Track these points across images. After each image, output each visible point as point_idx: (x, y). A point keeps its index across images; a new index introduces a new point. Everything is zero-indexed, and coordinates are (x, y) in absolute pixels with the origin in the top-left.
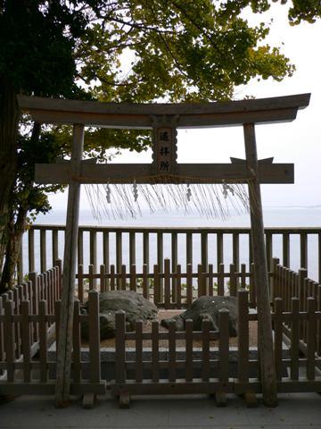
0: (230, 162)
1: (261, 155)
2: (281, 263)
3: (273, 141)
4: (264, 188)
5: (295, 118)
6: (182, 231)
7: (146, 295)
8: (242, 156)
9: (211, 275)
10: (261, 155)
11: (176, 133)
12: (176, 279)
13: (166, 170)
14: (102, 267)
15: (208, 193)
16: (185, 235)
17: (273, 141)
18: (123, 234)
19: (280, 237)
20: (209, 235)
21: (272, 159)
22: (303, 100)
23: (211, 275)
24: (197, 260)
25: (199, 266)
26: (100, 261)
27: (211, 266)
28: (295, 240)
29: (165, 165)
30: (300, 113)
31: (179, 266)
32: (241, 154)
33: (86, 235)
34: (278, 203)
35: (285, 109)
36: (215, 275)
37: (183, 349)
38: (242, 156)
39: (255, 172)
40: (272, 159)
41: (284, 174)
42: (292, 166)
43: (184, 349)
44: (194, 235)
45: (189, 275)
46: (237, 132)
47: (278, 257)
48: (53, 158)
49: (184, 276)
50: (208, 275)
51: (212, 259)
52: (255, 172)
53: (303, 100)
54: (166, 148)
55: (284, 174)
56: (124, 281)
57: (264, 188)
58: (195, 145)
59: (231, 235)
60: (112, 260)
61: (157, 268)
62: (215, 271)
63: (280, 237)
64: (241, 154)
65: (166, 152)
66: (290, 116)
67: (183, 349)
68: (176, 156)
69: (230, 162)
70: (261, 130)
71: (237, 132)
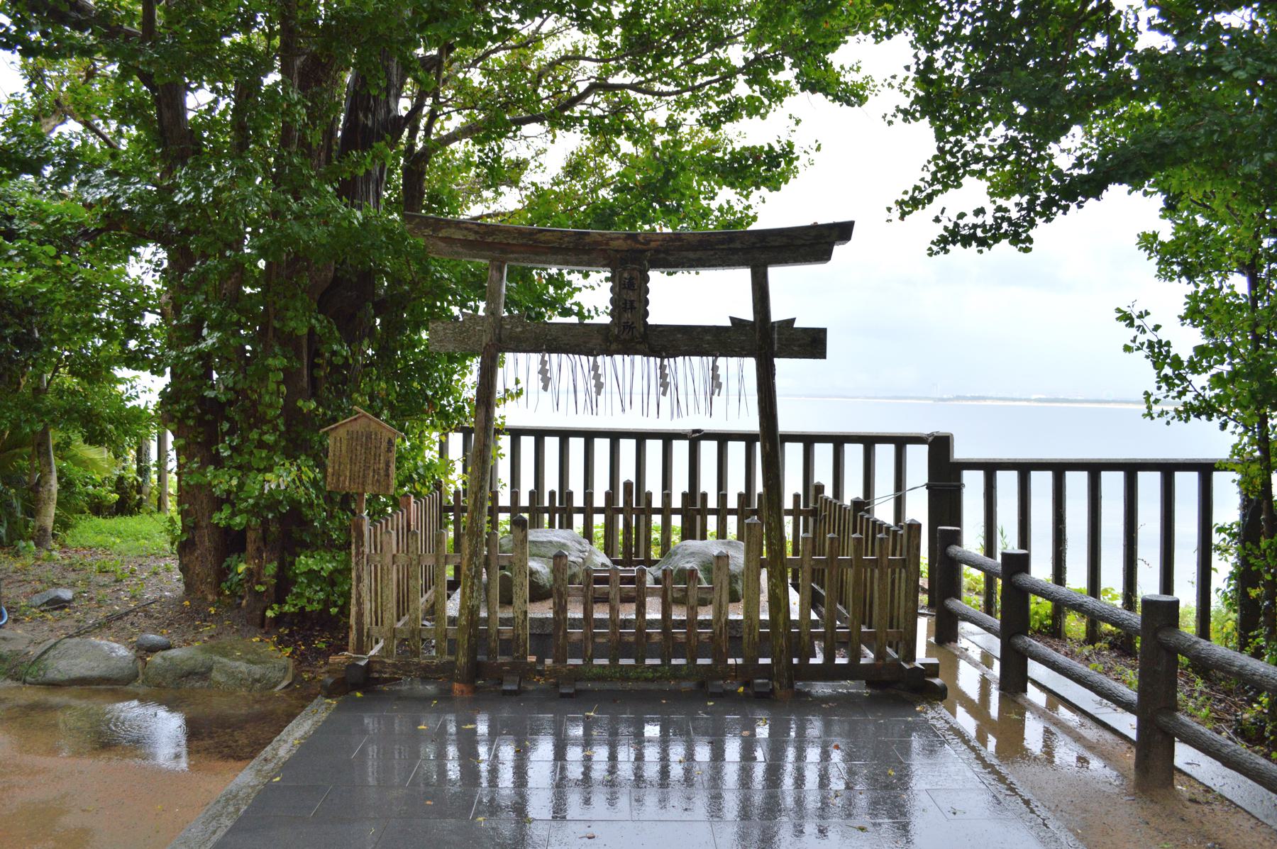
0: (729, 324)
1: (777, 315)
2: (828, 492)
3: (796, 293)
4: (781, 364)
5: (829, 259)
6: (552, 433)
7: (588, 533)
8: (748, 314)
9: (706, 512)
10: (777, 315)
11: (647, 279)
12: (643, 518)
13: (632, 333)
14: (531, 493)
15: (689, 370)
16: (582, 440)
17: (796, 293)
18: (523, 438)
19: (606, 442)
20: (846, 445)
21: (793, 320)
22: (843, 231)
23: (706, 512)
24: (680, 484)
25: (684, 495)
26: (527, 483)
27: (705, 496)
28: (853, 453)
29: (629, 327)
30: (838, 250)
31: (649, 495)
32: (747, 313)
33: (505, 442)
34: (805, 396)
35: (816, 243)
36: (620, 511)
37: (579, 614)
38: (748, 314)
39: (768, 341)
40: (793, 320)
41: (811, 343)
42: (823, 331)
43: (580, 615)
44: (675, 443)
45: (666, 511)
46: (743, 276)
47: (823, 482)
48: (1148, 140)
49: (657, 511)
50: (699, 512)
51: (708, 483)
52: (768, 341)
53: (843, 231)
54: (632, 302)
55: (811, 343)
56: (648, 522)
57: (781, 364)
58: (678, 298)
59: (634, 441)
60: (551, 482)
61: (611, 496)
62: (712, 503)
63: (606, 442)
64: (747, 313)
65: (632, 308)
66: (823, 255)
67: (579, 614)
68: (646, 314)
69: (729, 324)
70: (776, 274)
71: (743, 276)
